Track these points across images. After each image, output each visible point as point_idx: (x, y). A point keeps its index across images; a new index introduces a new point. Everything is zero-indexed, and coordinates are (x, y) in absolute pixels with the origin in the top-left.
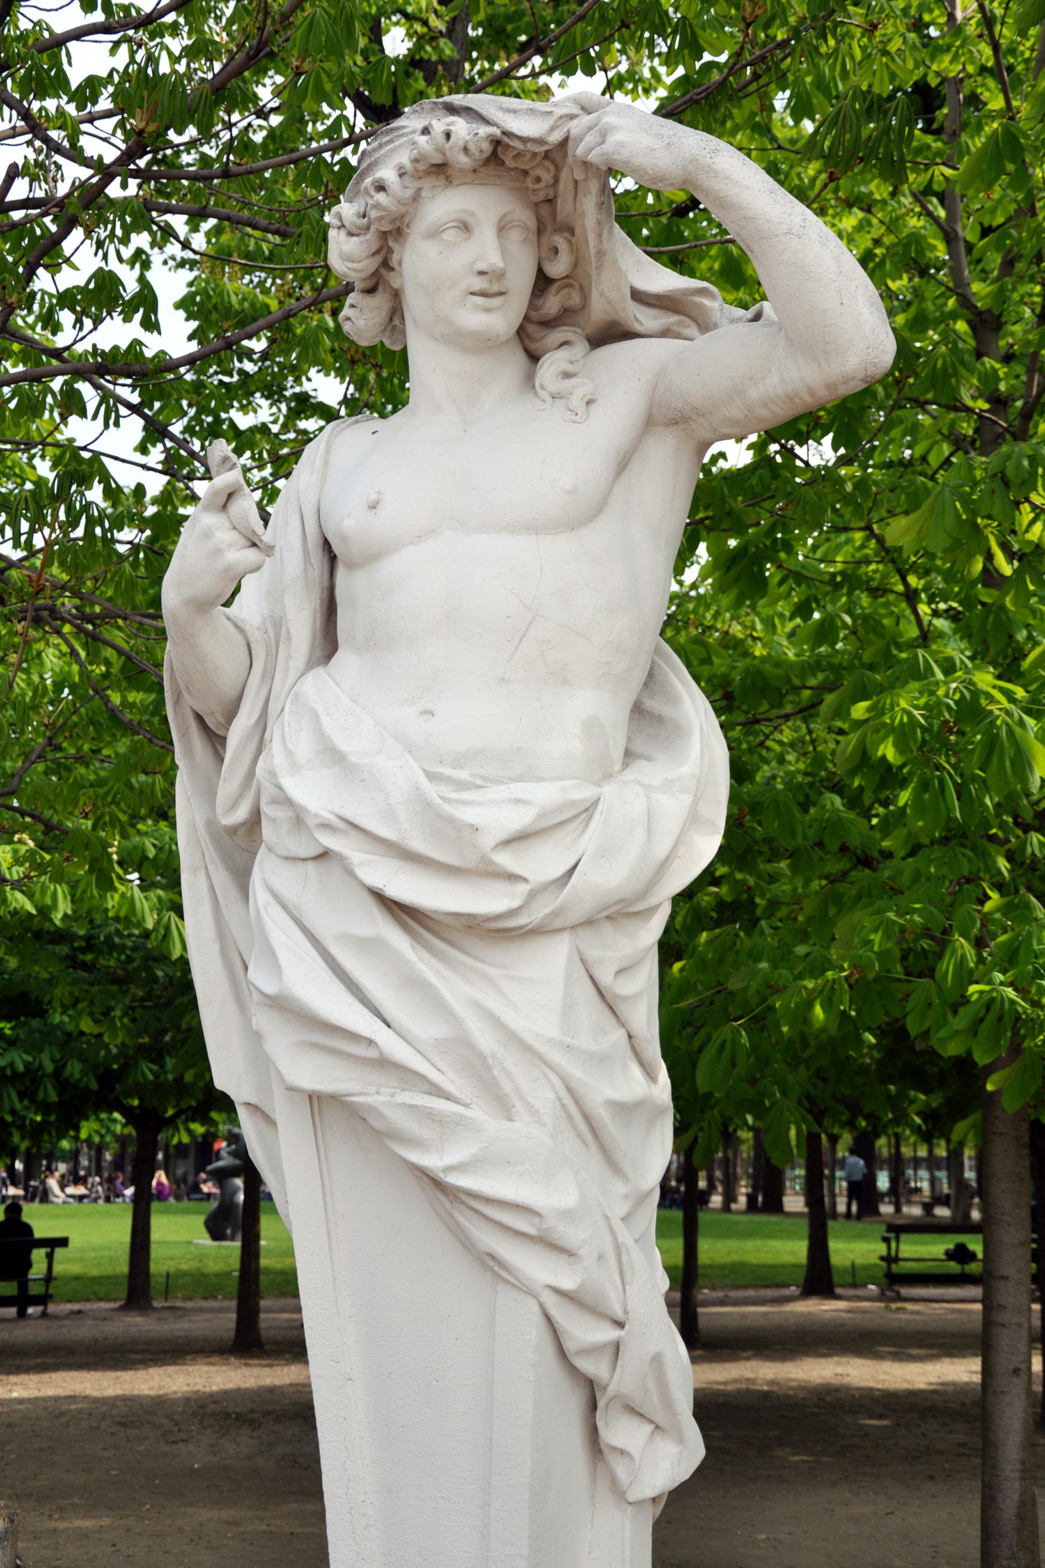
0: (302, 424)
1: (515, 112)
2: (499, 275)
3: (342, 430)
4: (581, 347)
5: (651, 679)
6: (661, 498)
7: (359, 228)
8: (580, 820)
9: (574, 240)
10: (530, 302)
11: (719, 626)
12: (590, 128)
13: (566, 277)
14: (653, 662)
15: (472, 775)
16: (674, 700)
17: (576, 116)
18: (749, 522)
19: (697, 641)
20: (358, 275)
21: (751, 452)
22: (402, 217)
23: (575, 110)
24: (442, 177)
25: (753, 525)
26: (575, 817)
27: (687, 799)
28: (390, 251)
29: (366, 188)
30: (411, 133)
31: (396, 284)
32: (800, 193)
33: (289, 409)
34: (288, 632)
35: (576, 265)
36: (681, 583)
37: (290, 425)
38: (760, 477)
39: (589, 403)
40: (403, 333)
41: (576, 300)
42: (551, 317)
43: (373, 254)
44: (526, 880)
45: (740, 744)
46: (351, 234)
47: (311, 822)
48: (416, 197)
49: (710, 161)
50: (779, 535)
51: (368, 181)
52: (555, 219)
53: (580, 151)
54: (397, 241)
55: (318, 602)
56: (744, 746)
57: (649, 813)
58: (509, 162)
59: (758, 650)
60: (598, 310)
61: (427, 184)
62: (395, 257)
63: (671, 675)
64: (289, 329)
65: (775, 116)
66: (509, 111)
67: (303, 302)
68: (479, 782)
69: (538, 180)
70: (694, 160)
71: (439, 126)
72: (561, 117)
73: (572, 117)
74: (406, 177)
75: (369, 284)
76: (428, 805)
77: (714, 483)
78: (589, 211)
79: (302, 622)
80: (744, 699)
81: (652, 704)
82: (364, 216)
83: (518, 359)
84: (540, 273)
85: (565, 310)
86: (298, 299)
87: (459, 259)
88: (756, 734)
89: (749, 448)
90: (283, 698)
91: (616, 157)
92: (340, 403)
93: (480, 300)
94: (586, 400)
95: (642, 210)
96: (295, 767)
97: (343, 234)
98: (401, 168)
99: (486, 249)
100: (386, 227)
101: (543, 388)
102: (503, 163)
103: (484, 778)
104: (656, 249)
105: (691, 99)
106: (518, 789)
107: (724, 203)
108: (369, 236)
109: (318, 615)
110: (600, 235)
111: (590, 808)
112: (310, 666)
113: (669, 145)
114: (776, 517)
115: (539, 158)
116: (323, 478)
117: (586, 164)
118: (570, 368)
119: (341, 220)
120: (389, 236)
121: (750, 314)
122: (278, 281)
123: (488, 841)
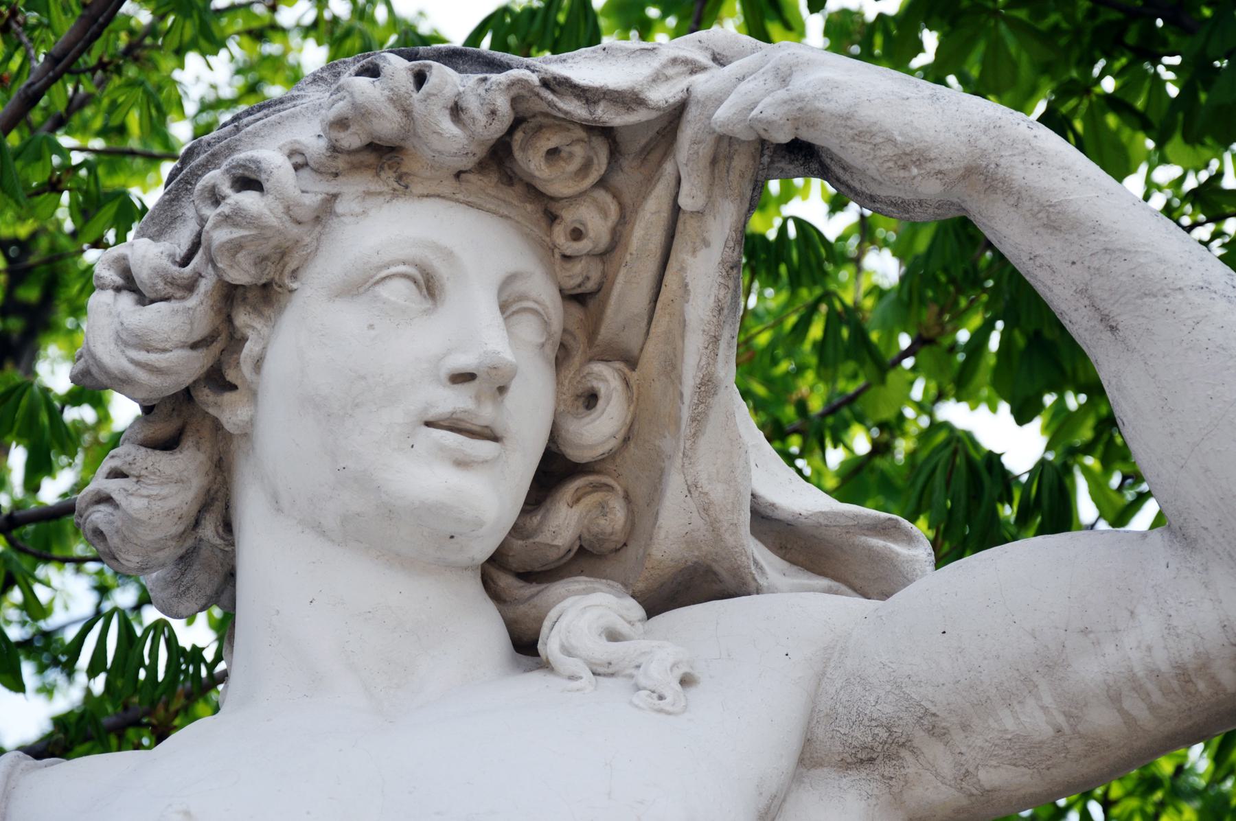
7: (171, 282)
9: (634, 376)
17: (704, 69)
24: (389, 175)
28: (236, 341)
42: (553, 555)
43: (194, 346)
48: (325, 213)
60: (673, 531)
61: (351, 188)
62: (250, 348)
72: (674, 61)
91: (821, 105)
94: (679, 673)
99: (478, 326)
100: (240, 275)
101: (567, 651)
108: (192, 302)
118: (623, 627)
120: (247, 297)
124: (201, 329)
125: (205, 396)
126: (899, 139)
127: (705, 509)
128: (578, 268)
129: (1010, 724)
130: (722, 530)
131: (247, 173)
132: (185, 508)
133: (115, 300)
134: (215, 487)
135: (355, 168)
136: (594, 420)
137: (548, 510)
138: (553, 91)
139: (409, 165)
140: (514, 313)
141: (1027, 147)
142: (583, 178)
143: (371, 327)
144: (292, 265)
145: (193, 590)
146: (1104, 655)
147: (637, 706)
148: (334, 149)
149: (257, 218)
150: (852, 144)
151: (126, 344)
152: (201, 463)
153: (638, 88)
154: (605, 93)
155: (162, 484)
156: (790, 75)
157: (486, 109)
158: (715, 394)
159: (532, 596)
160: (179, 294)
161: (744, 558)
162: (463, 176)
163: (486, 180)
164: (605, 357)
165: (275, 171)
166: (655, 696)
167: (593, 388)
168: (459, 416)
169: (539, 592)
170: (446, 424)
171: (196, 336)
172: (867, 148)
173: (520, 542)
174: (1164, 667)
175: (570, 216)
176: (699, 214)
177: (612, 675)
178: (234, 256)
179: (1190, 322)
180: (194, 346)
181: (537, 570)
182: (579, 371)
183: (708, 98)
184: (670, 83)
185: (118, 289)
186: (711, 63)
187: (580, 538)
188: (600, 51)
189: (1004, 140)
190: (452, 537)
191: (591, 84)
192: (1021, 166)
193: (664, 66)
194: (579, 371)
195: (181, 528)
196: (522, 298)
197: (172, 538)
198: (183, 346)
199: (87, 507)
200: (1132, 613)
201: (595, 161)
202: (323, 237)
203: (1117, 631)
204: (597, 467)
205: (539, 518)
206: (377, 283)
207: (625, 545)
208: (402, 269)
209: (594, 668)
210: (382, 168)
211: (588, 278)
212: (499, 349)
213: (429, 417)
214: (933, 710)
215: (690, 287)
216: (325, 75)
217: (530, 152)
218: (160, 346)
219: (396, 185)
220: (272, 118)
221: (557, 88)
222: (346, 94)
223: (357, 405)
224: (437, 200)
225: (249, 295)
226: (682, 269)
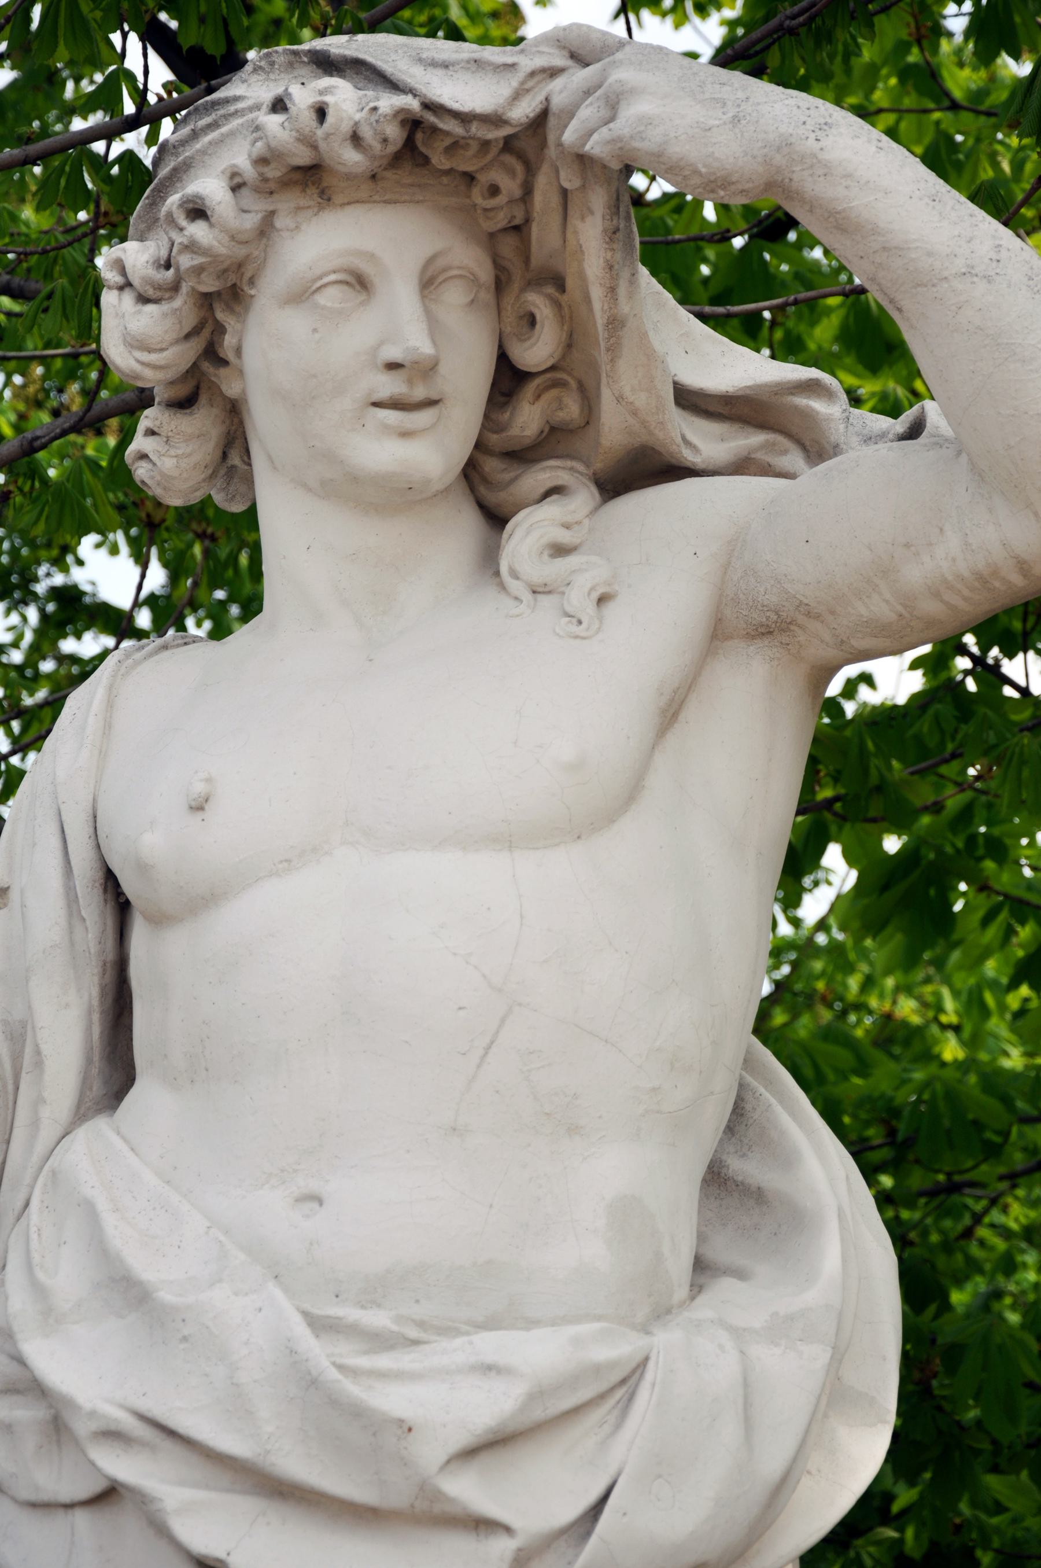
0: (68, 645)
1: (445, 65)
2: (426, 369)
3: (137, 663)
4: (583, 498)
5: (740, 1119)
6: (747, 763)
7: (158, 287)
8: (611, 1402)
9: (564, 299)
10: (486, 416)
11: (873, 1002)
12: (588, 93)
13: (553, 368)
14: (742, 1086)
15: (399, 1319)
16: (786, 1159)
18: (918, 803)
19: (834, 1035)
20: (160, 375)
21: (919, 674)
22: (240, 266)
23: (559, 60)
24: (312, 191)
25: (926, 809)
26: (602, 1397)
27: (819, 1355)
28: (220, 329)
29: (170, 215)
30: (251, 109)
31: (231, 389)
32: (992, 199)
33: (44, 616)
34: (38, 1052)
35: (569, 345)
36: (796, 922)
37: (46, 647)
38: (937, 720)
39: (602, 600)
40: (249, 481)
41: (572, 409)
42: (527, 442)
43: (188, 336)
44: (508, 1530)
45: (925, 1233)
46: (143, 299)
47: (82, 1428)
48: (266, 229)
49: (817, 146)
50: (983, 829)
51: (173, 200)
52: (527, 260)
53: (569, 136)
54: (229, 309)
55: (95, 992)
56: (934, 1238)
57: (746, 1384)
58: (439, 160)
59: (951, 1050)
61: (285, 204)
62: (229, 340)
63: (778, 1109)
64: (36, 473)
65: (945, 46)
66: (434, 64)
67: (65, 422)
68: (413, 1333)
69: (494, 190)
70: (786, 144)
71: (303, 95)
72: (532, 74)
73: (553, 73)
74: (245, 191)
75: (182, 391)
76: (313, 1383)
77: (848, 732)
78: (591, 244)
79: (63, 1031)
80: (921, 1152)
81: (744, 1167)
82: (168, 266)
83: (465, 523)
84: (503, 360)
86: (56, 413)
87: (353, 339)
88: (955, 1213)
89: (914, 665)
90: (28, 1180)
91: (637, 144)
92: (137, 604)
93: (391, 416)
94: (595, 595)
95: (694, 231)
96: (50, 1317)
97: (128, 299)
98: (234, 175)
99: (401, 320)
100: (209, 285)
101: (514, 575)
102: (426, 161)
103: (421, 1324)
104: (720, 310)
105: (780, 27)
106: (489, 1345)
107: (843, 223)
108: (178, 302)
109: (96, 1017)
110: (612, 290)
111: (629, 1379)
112: (81, 1115)
113: (736, 120)
114: (969, 795)
115: (494, 151)
116: (103, 755)
117: (583, 161)
118: (564, 537)
119: (123, 271)
120: (217, 302)
121: (900, 425)
122: (18, 379)
123: (430, 1453)
124: (190, 322)
126: (703, 170)
129: (863, 611)
130: (652, 427)
132: (208, 458)
133: (120, 299)
137: (514, 408)
139: (327, 181)
140: (441, 283)
141: (815, 161)
143: (315, 330)
144: (248, 275)
146: (922, 564)
147: (558, 635)
151: (132, 346)
152: (216, 416)
153: (500, 111)
156: (618, 103)
158: (624, 326)
160: (167, 295)
161: (674, 447)
163: (399, 172)
165: (216, 207)
166: (574, 620)
171: (187, 329)
174: (966, 574)
177: (550, 592)
178: (199, 274)
179: (954, 308)
182: (518, 297)
183: (562, 111)
185: (121, 288)
186: (569, 63)
189: (795, 157)
191: (461, 109)
192: (810, 179)
193: (523, 83)
195: (210, 471)
196: (445, 270)
197: (204, 480)
198: (177, 341)
199: (133, 463)
200: (941, 530)
203: (930, 544)
205: (508, 414)
207: (588, 423)
208: (333, 277)
209: (535, 589)
210: (307, 185)
212: (418, 344)
213: (373, 400)
214: (806, 601)
216: (263, 63)
218: (159, 346)
219: (320, 200)
223: (313, 398)
224: (358, 205)
226: (576, 232)
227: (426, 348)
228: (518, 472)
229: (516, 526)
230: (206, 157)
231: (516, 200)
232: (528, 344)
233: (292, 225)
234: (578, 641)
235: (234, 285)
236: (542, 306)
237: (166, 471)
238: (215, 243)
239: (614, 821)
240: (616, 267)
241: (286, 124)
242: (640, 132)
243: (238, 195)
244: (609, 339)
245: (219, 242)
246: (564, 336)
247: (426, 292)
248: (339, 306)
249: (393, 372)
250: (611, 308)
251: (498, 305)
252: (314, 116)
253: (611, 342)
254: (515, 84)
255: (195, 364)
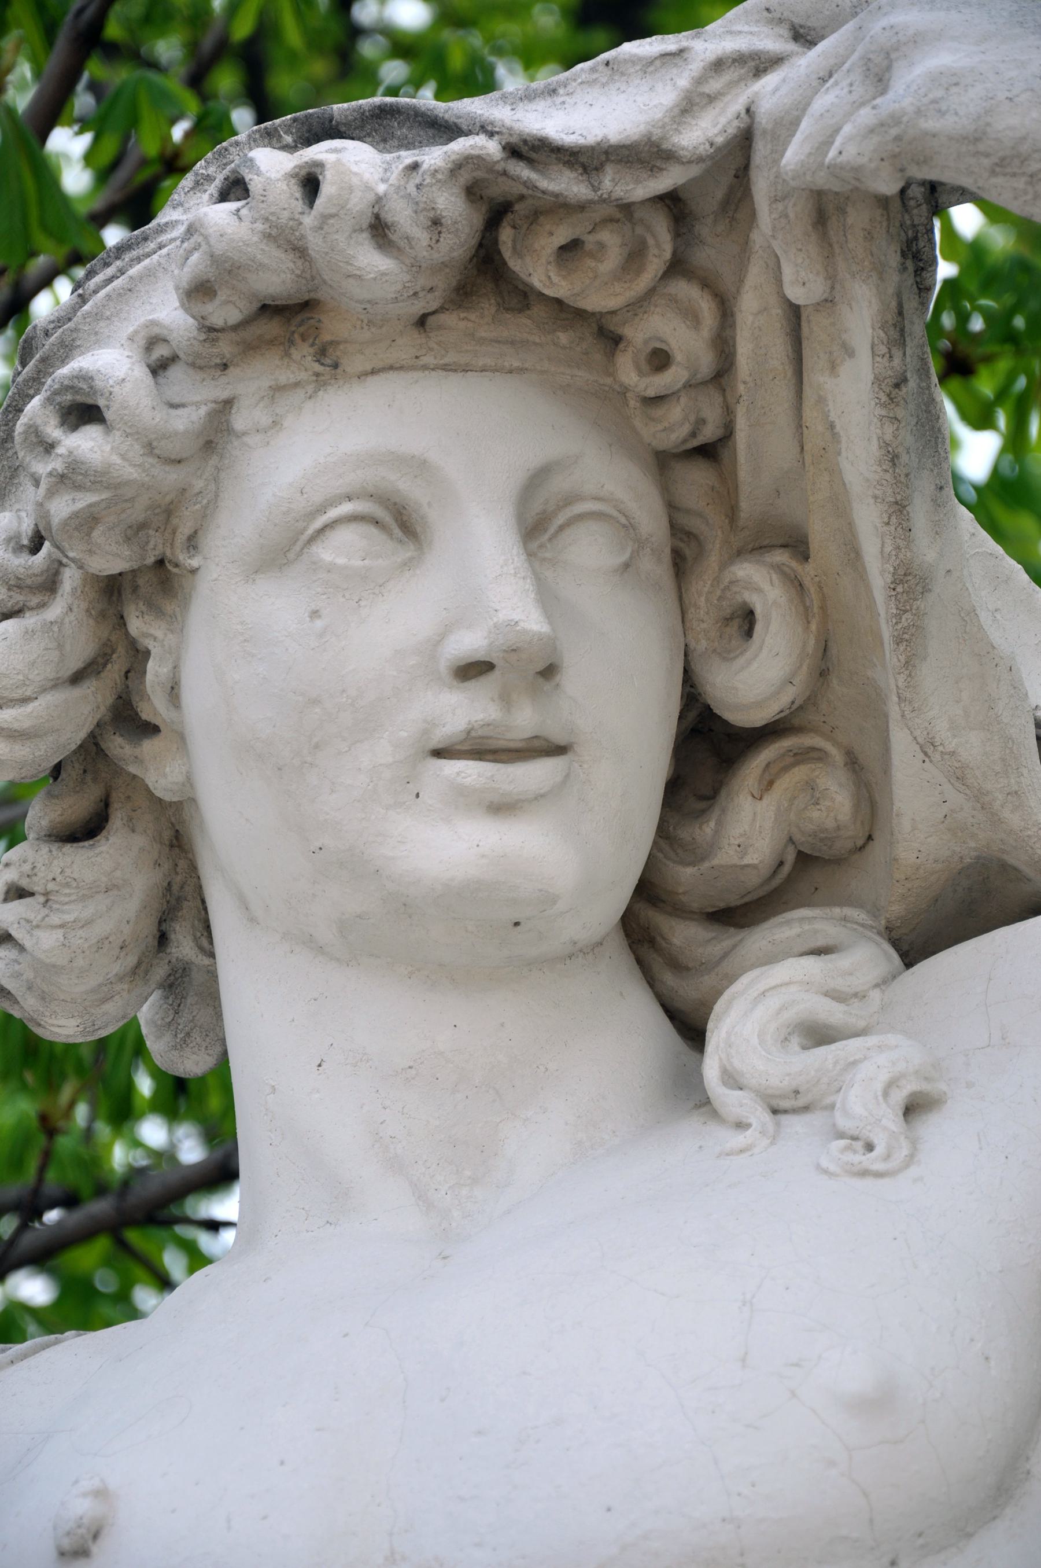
4: (866, 959)
7: (17, 585)
9: (808, 572)
24: (303, 352)
28: (139, 655)
39: (913, 1109)
41: (837, 802)
42: (753, 880)
43: (76, 678)
48: (216, 436)
52: (732, 513)
54: (155, 609)
61: (250, 383)
62: (155, 670)
72: (718, 65)
73: (760, 64)
74: (176, 372)
83: (634, 1023)
85: (804, 860)
91: (930, 124)
93: (470, 772)
94: (899, 1097)
98: (152, 342)
99: (483, 584)
100: (112, 559)
101: (732, 1080)
108: (55, 610)
110: (899, 508)
118: (832, 1013)
124: (80, 650)
125: (118, 746)
127: (959, 776)
128: (676, 412)
130: (997, 806)
131: (80, 399)
132: (127, 930)
134: (179, 879)
135: (251, 348)
136: (749, 663)
137: (724, 811)
138: (530, 162)
139: (333, 328)
140: (561, 528)
142: (639, 272)
143: (315, 614)
145: (196, 1035)
147: (826, 1172)
148: (210, 331)
149: (104, 473)
150: (994, 181)
152: (142, 850)
153: (657, 133)
154: (606, 153)
155: (83, 898)
156: (889, 68)
157: (424, 219)
158: (926, 590)
159: (726, 955)
160: (34, 601)
162: (431, 320)
163: (473, 316)
164: (755, 546)
165: (116, 389)
166: (859, 1145)
167: (745, 603)
168: (480, 733)
169: (735, 946)
170: (466, 747)
171: (75, 664)
172: (1020, 183)
173: (689, 870)
175: (640, 333)
176: (828, 303)
177: (806, 1109)
180: (76, 678)
181: (733, 904)
182: (717, 580)
184: (719, 105)
186: (791, 47)
187: (791, 840)
188: (601, 68)
190: (517, 924)
191: (582, 141)
193: (699, 81)
194: (717, 580)
195: (131, 960)
196: (570, 500)
197: (121, 978)
198: (55, 685)
201: (651, 241)
202: (222, 475)
204: (796, 722)
206: (312, 540)
207: (870, 838)
208: (346, 508)
210: (291, 342)
211: (703, 421)
213: (435, 742)
215: (838, 429)
217: (528, 259)
218: (17, 694)
219: (318, 368)
220: (135, 271)
221: (533, 155)
222: (200, 239)
223: (317, 746)
224: (392, 375)
225: (141, 582)
226: (821, 400)
227: (532, 621)
228: (739, 938)
229: (730, 1003)
230: (102, 324)
231: (704, 383)
232: (741, 661)
233: (265, 420)
234: (869, 1182)
235: (161, 563)
236: (766, 586)
237: (42, 956)
238: (116, 459)
239: (970, 1536)
240: (904, 458)
241: (244, 212)
242: (934, 101)
243: (161, 380)
244: (898, 617)
245: (123, 457)
246: (812, 642)
247: (534, 545)
248: (359, 563)
249: (472, 684)
250: (898, 548)
251: (681, 599)
252: (298, 192)
253: (904, 623)
254: (684, 81)
255: (92, 735)
